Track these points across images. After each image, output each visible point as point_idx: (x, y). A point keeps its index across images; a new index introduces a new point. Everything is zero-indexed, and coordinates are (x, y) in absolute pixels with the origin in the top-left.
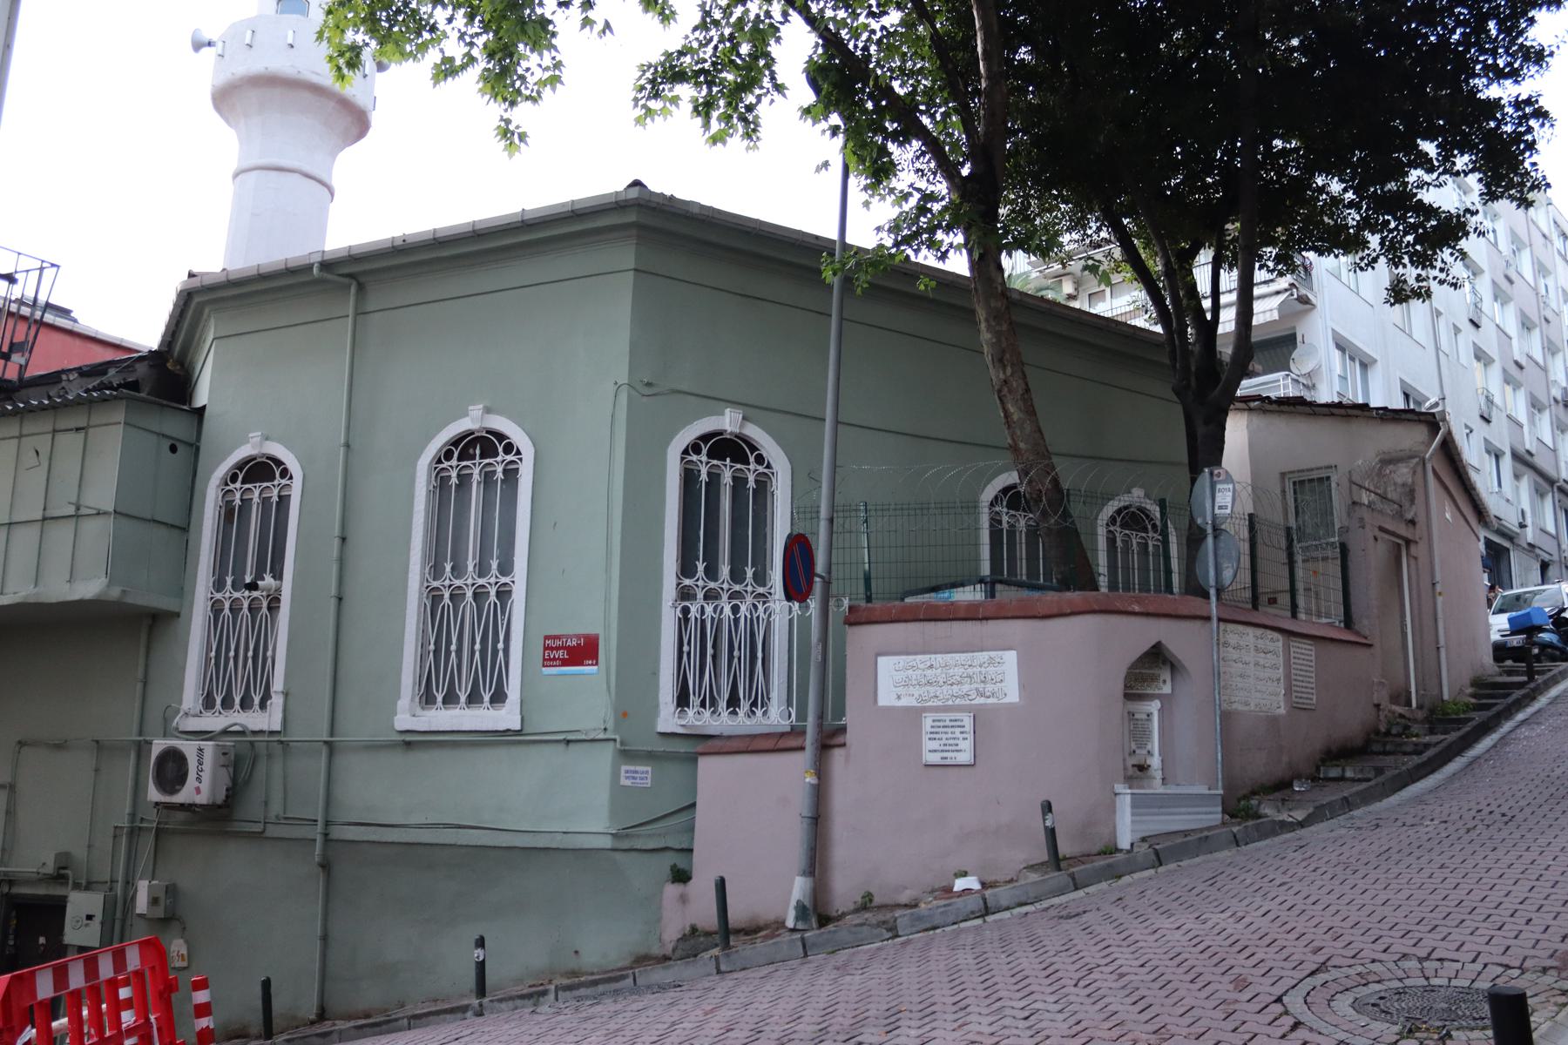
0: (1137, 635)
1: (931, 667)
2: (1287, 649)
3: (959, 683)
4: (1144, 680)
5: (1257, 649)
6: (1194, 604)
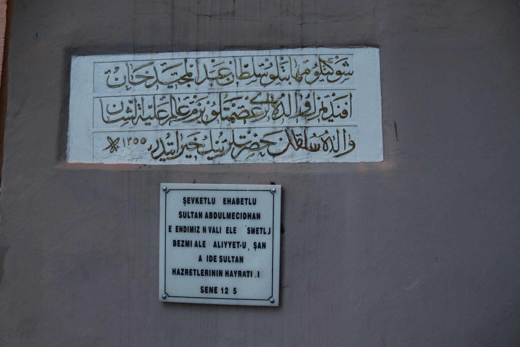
3: (249, 116)
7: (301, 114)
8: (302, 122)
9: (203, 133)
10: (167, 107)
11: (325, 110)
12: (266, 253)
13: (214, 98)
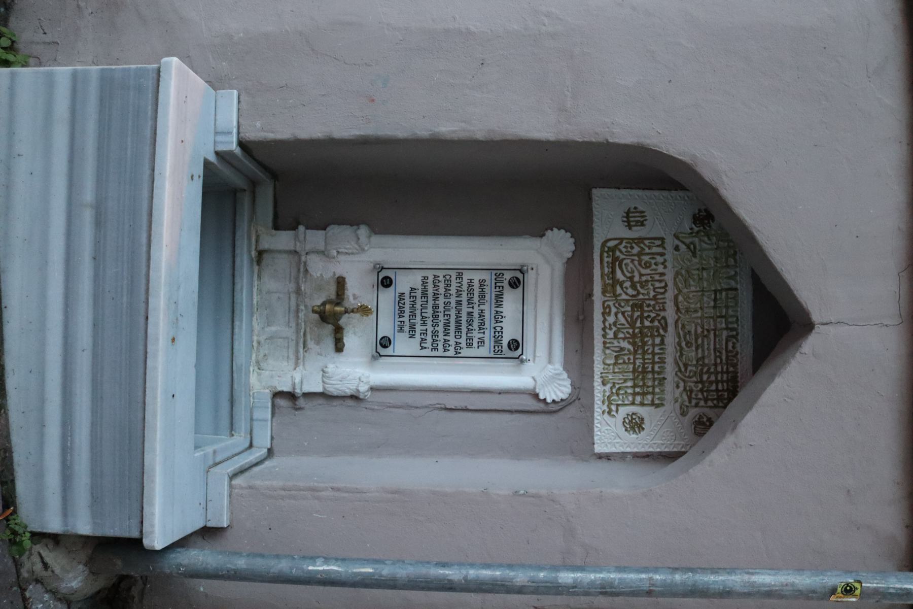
4: (639, 340)
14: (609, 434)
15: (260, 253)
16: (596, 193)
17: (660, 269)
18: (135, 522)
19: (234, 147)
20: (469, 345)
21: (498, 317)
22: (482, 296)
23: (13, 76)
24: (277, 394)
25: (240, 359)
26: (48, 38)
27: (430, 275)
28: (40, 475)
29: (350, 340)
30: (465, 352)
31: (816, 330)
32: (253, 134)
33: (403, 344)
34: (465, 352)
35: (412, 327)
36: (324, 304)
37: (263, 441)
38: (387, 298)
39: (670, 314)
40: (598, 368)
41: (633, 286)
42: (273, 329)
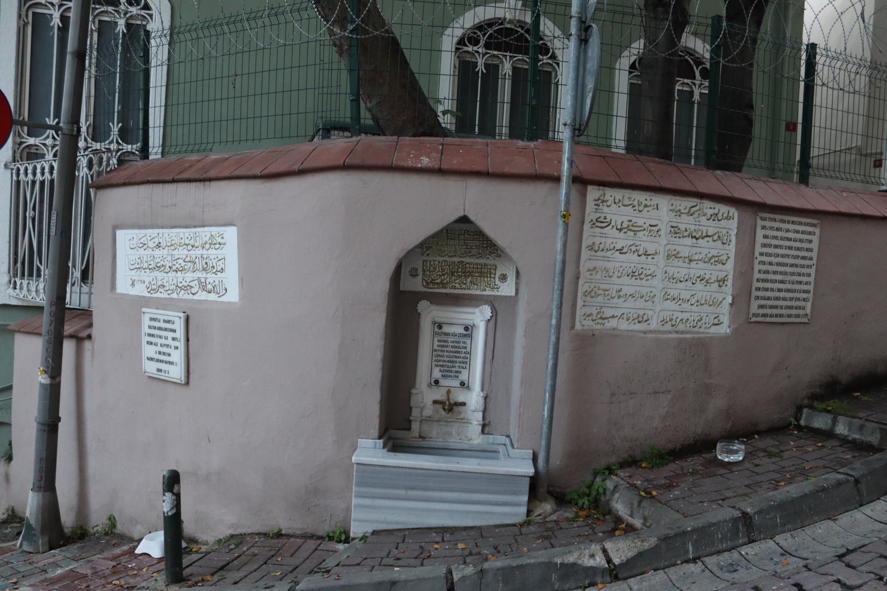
0: (414, 205)
1: (159, 246)
2: (746, 236)
3: (183, 270)
4: (467, 274)
5: (675, 231)
6: (522, 153)
7: (204, 270)
8: (204, 275)
9: (166, 279)
10: (152, 262)
11: (213, 267)
12: (178, 351)
13: (169, 258)
14: (507, 289)
15: (420, 437)
16: (402, 289)
17: (437, 263)
18: (524, 479)
19: (381, 441)
20: (466, 348)
21: (454, 335)
22: (445, 341)
23: (354, 520)
24: (483, 432)
25: (466, 447)
26: (328, 519)
27: (434, 363)
28: (505, 514)
29: (461, 399)
30: (468, 350)
31: (466, 213)
32: (375, 432)
33: (464, 376)
34: (468, 350)
35: (456, 372)
36: (444, 410)
37: (503, 439)
38: (443, 382)
39: (457, 259)
40: (478, 292)
41: (444, 275)
42: (454, 432)
